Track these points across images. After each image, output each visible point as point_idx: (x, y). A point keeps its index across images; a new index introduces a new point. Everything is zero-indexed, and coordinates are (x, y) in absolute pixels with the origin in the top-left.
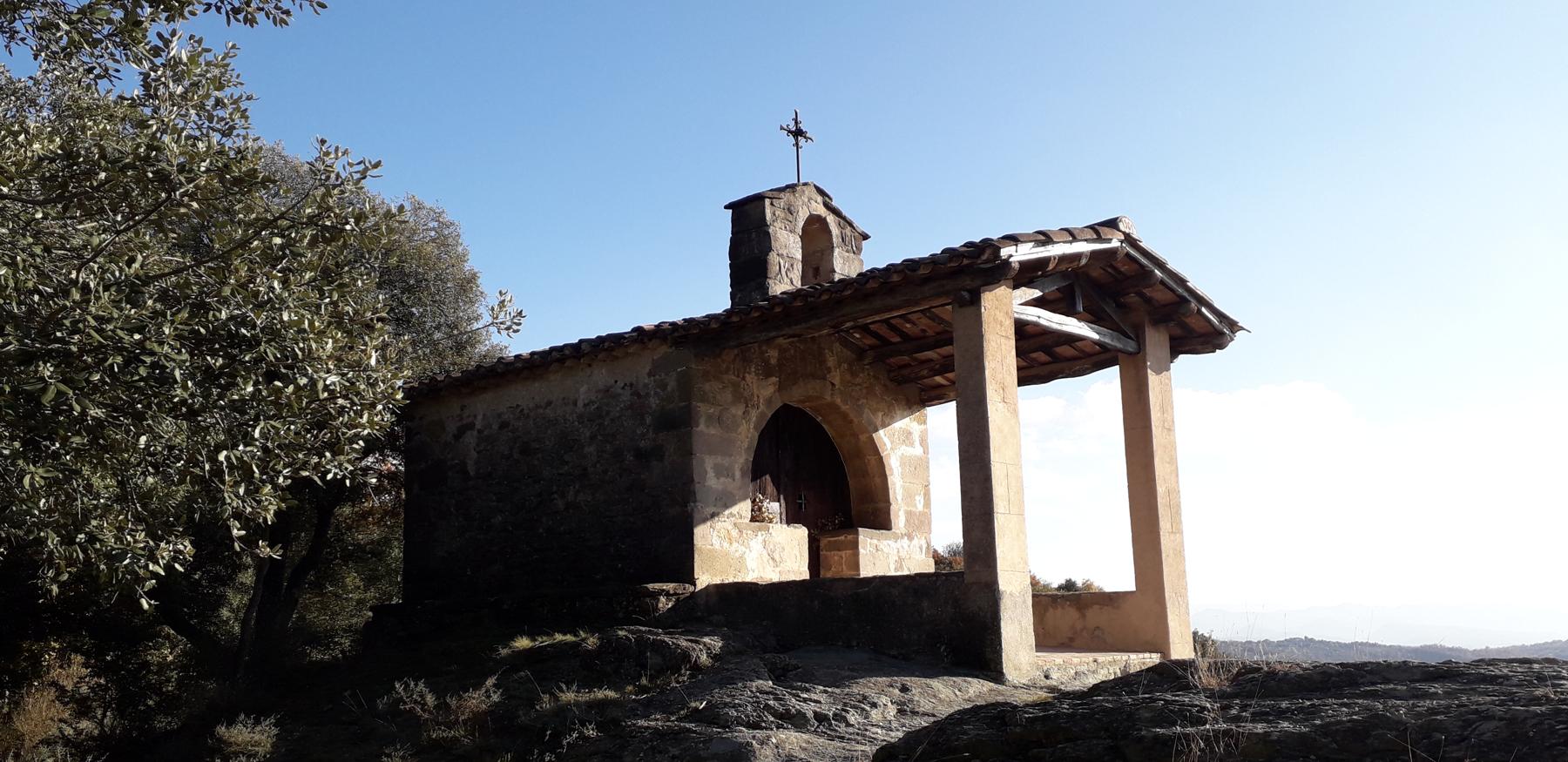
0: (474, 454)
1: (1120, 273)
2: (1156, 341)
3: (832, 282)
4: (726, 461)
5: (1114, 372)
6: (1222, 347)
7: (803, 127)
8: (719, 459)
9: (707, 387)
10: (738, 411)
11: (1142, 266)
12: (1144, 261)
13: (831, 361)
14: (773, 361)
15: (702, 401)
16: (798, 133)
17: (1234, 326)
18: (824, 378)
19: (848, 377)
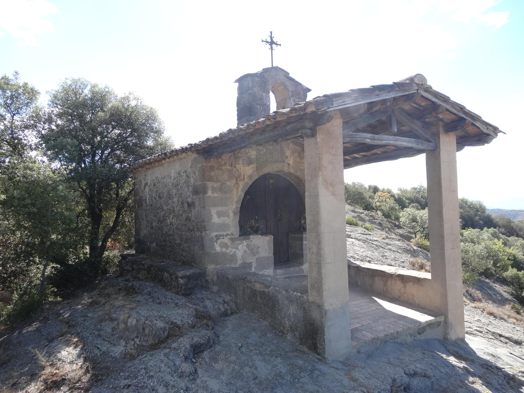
0: (148, 196)
1: (423, 106)
2: (447, 141)
3: (268, 117)
4: (224, 209)
5: (423, 157)
6: (487, 142)
7: (275, 40)
8: (220, 208)
9: (213, 174)
10: (230, 183)
11: (433, 103)
12: (434, 100)
13: (288, 153)
14: (253, 157)
15: (209, 181)
16: (272, 43)
17: (496, 130)
18: (284, 162)
19: (298, 160)
